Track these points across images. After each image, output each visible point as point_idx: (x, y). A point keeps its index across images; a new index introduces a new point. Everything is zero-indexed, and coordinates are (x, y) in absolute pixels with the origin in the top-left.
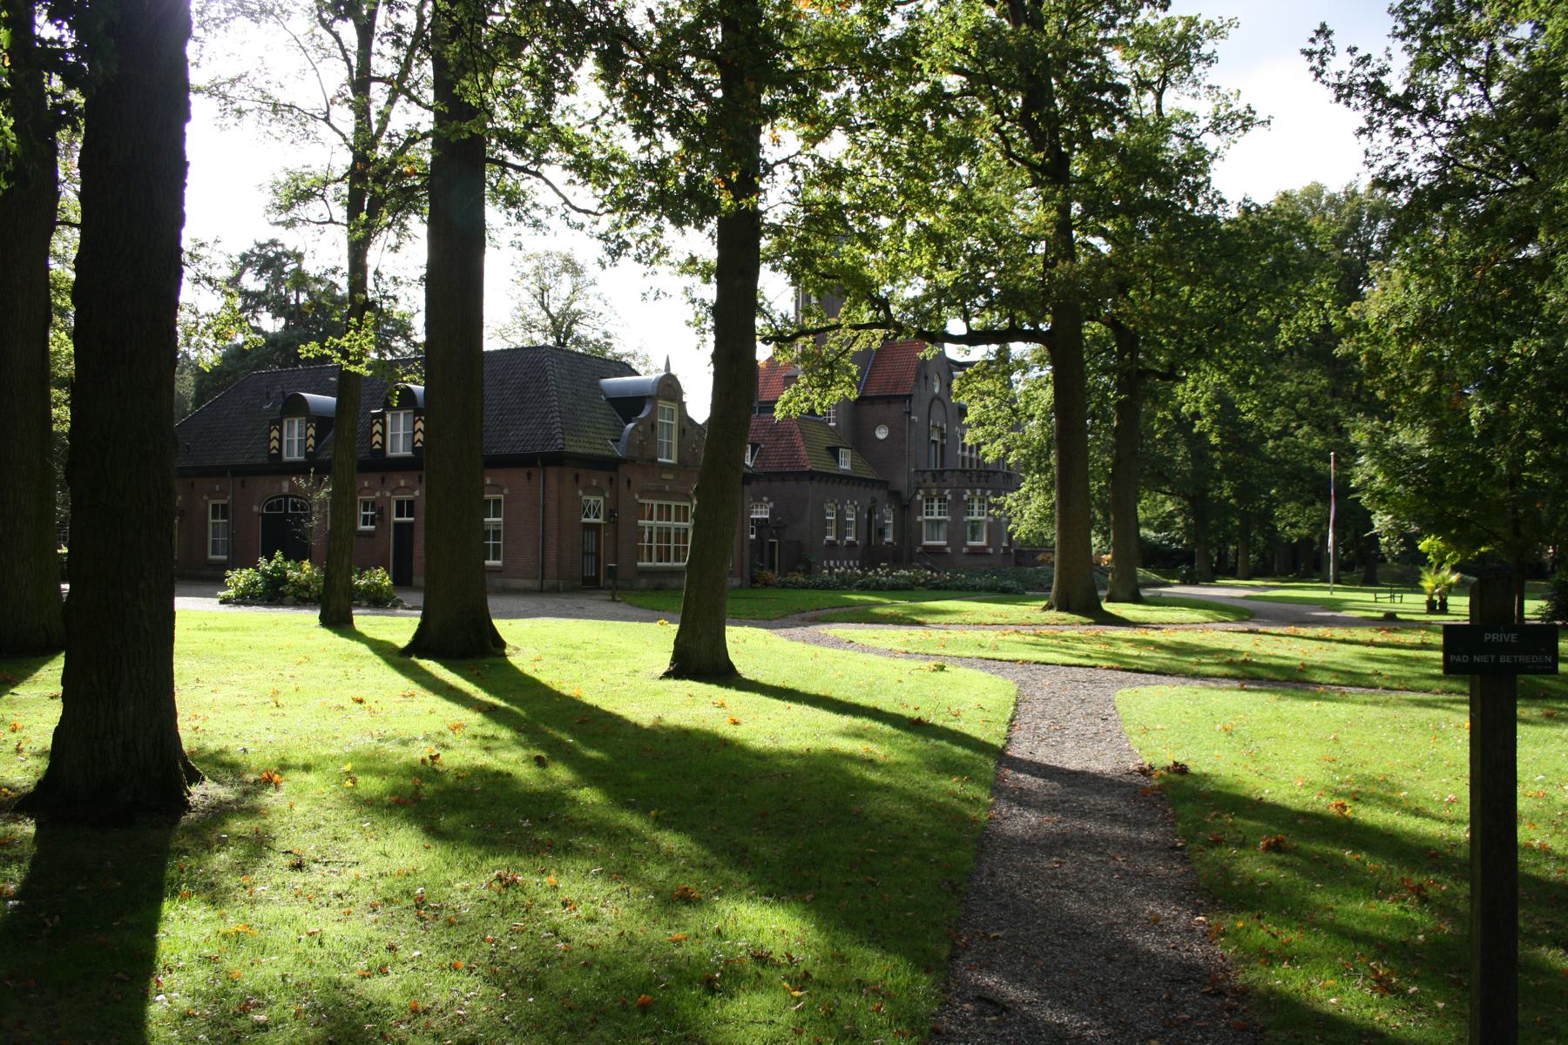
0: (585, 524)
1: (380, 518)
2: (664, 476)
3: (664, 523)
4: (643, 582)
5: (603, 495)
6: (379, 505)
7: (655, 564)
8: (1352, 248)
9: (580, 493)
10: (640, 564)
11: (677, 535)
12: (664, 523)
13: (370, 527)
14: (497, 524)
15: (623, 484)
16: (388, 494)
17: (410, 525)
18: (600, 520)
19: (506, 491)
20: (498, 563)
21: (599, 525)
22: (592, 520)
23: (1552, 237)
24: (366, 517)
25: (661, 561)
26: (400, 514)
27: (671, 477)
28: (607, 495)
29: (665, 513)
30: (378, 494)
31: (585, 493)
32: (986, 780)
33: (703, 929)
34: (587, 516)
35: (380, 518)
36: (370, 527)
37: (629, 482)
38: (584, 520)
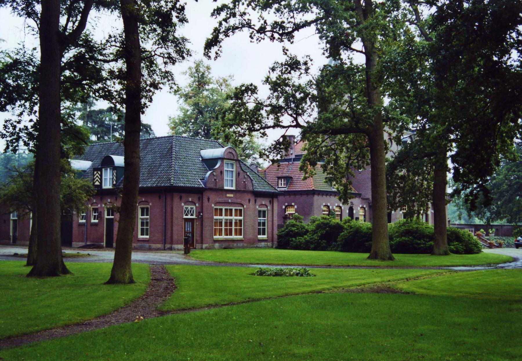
0: (186, 219)
1: (100, 217)
2: (228, 195)
3: (229, 217)
4: (217, 245)
5: (195, 204)
6: (99, 210)
7: (223, 237)
8: (339, 33)
9: (183, 204)
10: (215, 237)
11: (236, 223)
12: (229, 217)
13: (96, 221)
14: (147, 219)
15: (205, 200)
16: (103, 205)
17: (112, 219)
18: (194, 217)
19: (151, 204)
20: (148, 237)
21: (193, 219)
22: (189, 217)
23: (104, 74)
24: (95, 216)
25: (227, 235)
26: (108, 215)
27: (232, 195)
28: (197, 205)
29: (229, 212)
30: (99, 206)
31: (185, 204)
32: (164, 40)
33: (197, 134)
34: (186, 215)
35: (100, 217)
36: (96, 221)
37: (209, 199)
38: (185, 217)
